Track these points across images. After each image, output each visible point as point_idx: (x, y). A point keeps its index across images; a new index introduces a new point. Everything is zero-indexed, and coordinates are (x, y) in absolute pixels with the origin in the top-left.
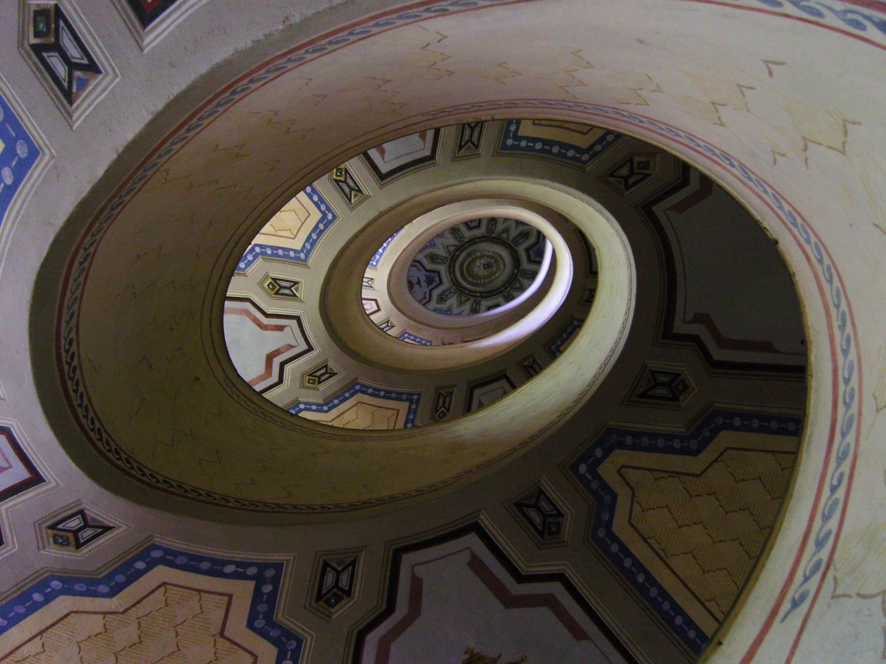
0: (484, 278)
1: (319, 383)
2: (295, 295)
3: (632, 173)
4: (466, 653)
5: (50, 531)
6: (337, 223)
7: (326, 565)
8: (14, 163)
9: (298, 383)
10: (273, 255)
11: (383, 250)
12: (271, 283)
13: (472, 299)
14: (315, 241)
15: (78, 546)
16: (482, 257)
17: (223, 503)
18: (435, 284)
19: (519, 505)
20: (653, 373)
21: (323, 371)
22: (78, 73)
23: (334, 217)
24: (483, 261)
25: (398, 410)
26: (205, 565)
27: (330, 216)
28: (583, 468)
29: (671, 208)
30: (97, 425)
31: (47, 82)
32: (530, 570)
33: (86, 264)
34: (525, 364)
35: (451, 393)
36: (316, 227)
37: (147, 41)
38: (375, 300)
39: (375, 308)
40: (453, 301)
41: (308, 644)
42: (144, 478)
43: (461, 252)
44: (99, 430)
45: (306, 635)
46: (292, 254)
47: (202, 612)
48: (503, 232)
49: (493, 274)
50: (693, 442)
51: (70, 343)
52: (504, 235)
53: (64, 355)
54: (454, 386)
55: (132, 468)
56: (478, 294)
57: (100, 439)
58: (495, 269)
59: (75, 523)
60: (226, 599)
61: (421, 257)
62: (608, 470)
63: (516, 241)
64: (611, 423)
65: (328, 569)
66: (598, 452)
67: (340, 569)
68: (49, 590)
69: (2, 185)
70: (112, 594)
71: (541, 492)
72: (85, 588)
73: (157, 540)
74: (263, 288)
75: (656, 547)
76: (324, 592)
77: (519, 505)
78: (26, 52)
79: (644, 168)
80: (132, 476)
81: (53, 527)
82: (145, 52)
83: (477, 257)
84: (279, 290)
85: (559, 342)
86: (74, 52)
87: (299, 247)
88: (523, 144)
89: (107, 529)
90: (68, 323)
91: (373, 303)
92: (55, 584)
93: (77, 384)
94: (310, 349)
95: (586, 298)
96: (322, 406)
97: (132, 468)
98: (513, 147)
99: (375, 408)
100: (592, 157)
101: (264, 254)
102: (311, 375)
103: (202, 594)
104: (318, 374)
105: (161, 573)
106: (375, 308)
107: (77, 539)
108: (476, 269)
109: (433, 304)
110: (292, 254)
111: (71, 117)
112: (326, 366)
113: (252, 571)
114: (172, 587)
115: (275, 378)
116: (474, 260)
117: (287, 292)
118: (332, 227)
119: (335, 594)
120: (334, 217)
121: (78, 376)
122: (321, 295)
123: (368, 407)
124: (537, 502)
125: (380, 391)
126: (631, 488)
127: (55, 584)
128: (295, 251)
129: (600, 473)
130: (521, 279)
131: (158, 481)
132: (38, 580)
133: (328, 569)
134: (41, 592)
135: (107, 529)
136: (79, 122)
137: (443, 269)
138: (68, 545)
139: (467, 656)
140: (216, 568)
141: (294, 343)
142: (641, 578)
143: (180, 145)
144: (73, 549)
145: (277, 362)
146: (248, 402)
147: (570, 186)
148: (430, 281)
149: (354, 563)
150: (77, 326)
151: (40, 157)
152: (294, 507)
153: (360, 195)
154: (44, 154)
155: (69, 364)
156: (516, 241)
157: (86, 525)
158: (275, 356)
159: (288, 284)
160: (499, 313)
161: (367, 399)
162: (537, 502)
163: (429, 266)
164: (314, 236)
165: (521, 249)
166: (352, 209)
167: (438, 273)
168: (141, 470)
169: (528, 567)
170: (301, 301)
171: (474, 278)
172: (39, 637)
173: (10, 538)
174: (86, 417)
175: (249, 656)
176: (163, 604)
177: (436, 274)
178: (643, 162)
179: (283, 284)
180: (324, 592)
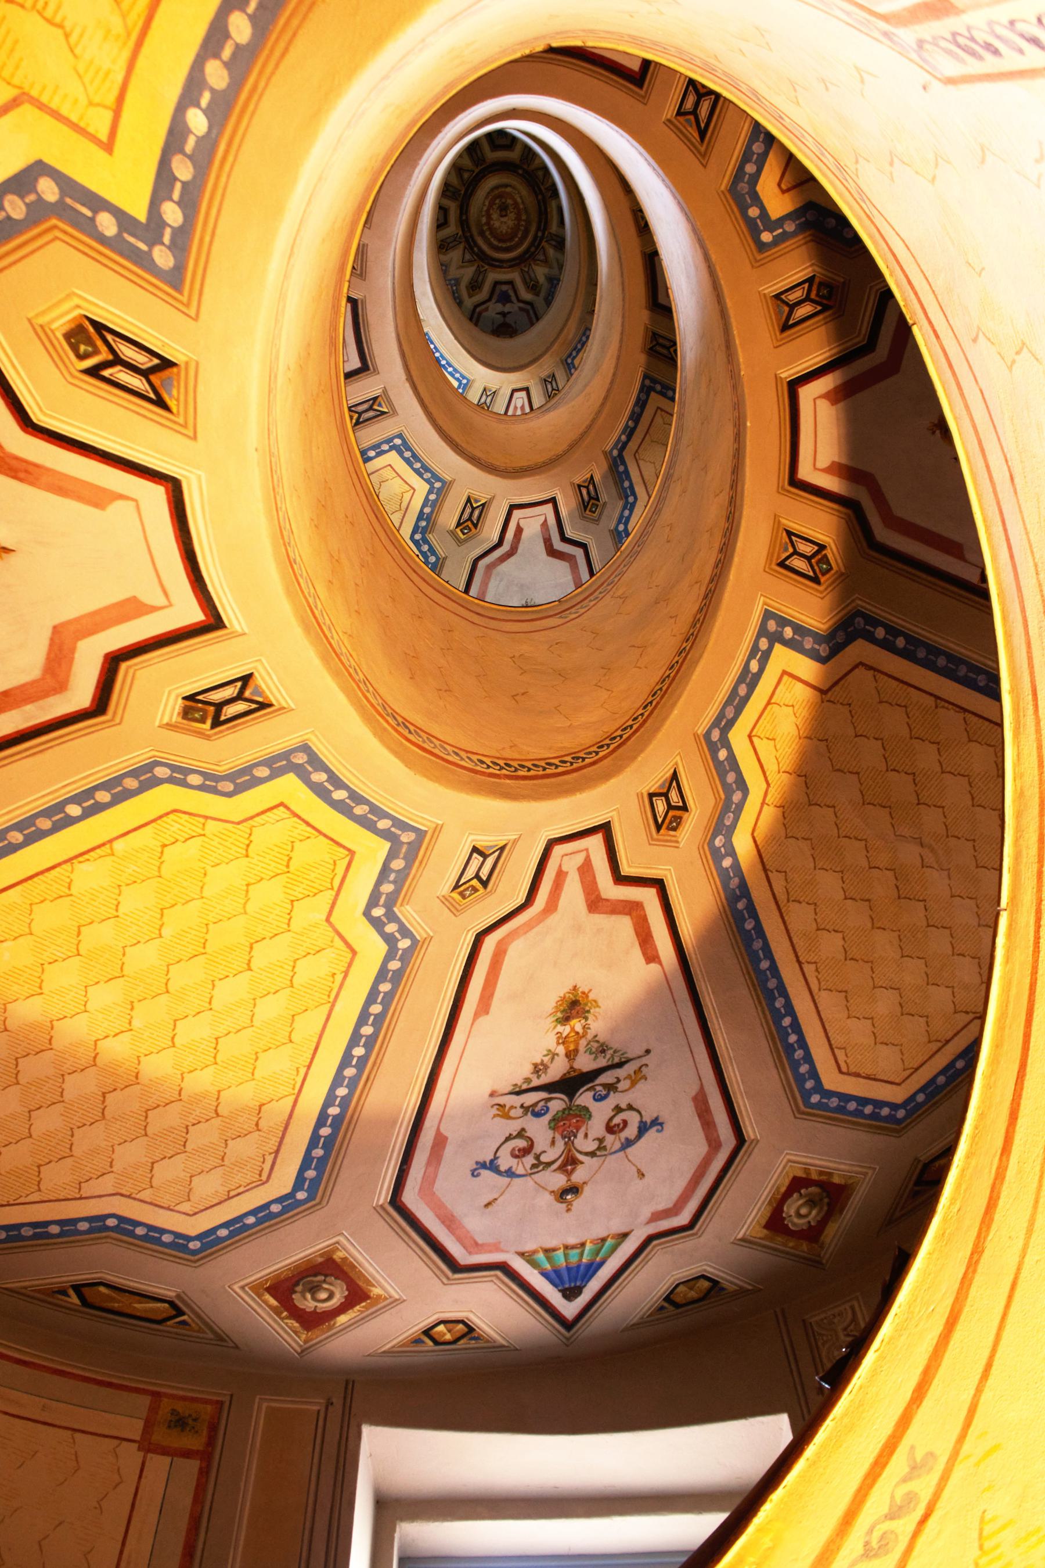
0: (518, 218)
1: (598, 499)
2: (483, 505)
4: (934, 433)
5: (662, 831)
6: (407, 435)
7: (782, 564)
8: (310, 769)
9: (592, 526)
11: (450, 366)
13: (544, 244)
15: (685, 808)
16: (489, 217)
17: (683, 655)
18: (511, 293)
19: (785, 327)
20: (680, 113)
22: (247, 694)
23: (400, 436)
24: (495, 216)
25: (658, 408)
26: (742, 690)
27: (398, 441)
28: (766, 237)
30: (569, 759)
31: (247, 721)
32: (863, 332)
33: (412, 728)
36: (407, 461)
37: (238, 628)
38: (514, 391)
39: (523, 394)
40: (540, 272)
41: (864, 604)
42: (635, 727)
43: (476, 244)
44: (573, 758)
45: (854, 605)
46: (432, 497)
47: (793, 706)
48: (461, 177)
49: (516, 203)
51: (482, 762)
52: (466, 175)
53: (491, 770)
55: (621, 736)
57: (584, 759)
58: (509, 201)
59: (661, 806)
60: (786, 678)
61: (469, 303)
64: (723, 188)
65: (787, 563)
66: (754, 212)
67: (791, 550)
68: (723, 850)
70: (745, 791)
71: (777, 297)
72: (731, 815)
73: (701, 730)
74: (465, 541)
76: (811, 574)
77: (785, 327)
78: (216, 734)
80: (629, 738)
81: (659, 827)
82: (246, 631)
83: (488, 223)
84: (472, 522)
86: (229, 692)
87: (427, 487)
89: (675, 776)
90: (462, 759)
91: (516, 395)
92: (719, 842)
93: (523, 766)
96: (627, 502)
97: (621, 736)
102: (585, 508)
103: (773, 701)
105: (737, 737)
106: (523, 394)
107: (678, 808)
108: (504, 229)
109: (539, 302)
110: (432, 497)
111: (284, 708)
112: (579, 486)
113: (764, 644)
114: (755, 730)
115: (578, 552)
116: (491, 229)
117: (477, 513)
118: (411, 441)
119: (818, 563)
120: (400, 436)
121: (515, 764)
122: (490, 473)
123: (642, 446)
124: (787, 304)
127: (719, 842)
128: (430, 492)
130: (532, 167)
131: (642, 715)
132: (709, 857)
133: (787, 563)
134: (723, 857)
135: (675, 776)
136: (290, 701)
137: (493, 276)
138: (681, 818)
139: (938, 432)
140: (749, 680)
141: (542, 518)
143: (326, 618)
144: (685, 815)
145: (558, 545)
146: (592, 598)
147: (428, 146)
148: (505, 298)
149: (790, 534)
150: (467, 752)
151: (310, 744)
152: (711, 581)
154: (858, 605)
155: (502, 768)
157: (666, 795)
158: (551, 545)
159: (468, 510)
160: (571, 221)
161: (632, 445)
162: (787, 304)
164: (418, 465)
166: (395, 412)
167: (496, 283)
168: (625, 729)
169: (859, 334)
171: (516, 236)
172: (769, 873)
173: (659, 872)
174: (557, 767)
175: (857, 670)
176: (772, 742)
179: (466, 516)
180: (811, 574)
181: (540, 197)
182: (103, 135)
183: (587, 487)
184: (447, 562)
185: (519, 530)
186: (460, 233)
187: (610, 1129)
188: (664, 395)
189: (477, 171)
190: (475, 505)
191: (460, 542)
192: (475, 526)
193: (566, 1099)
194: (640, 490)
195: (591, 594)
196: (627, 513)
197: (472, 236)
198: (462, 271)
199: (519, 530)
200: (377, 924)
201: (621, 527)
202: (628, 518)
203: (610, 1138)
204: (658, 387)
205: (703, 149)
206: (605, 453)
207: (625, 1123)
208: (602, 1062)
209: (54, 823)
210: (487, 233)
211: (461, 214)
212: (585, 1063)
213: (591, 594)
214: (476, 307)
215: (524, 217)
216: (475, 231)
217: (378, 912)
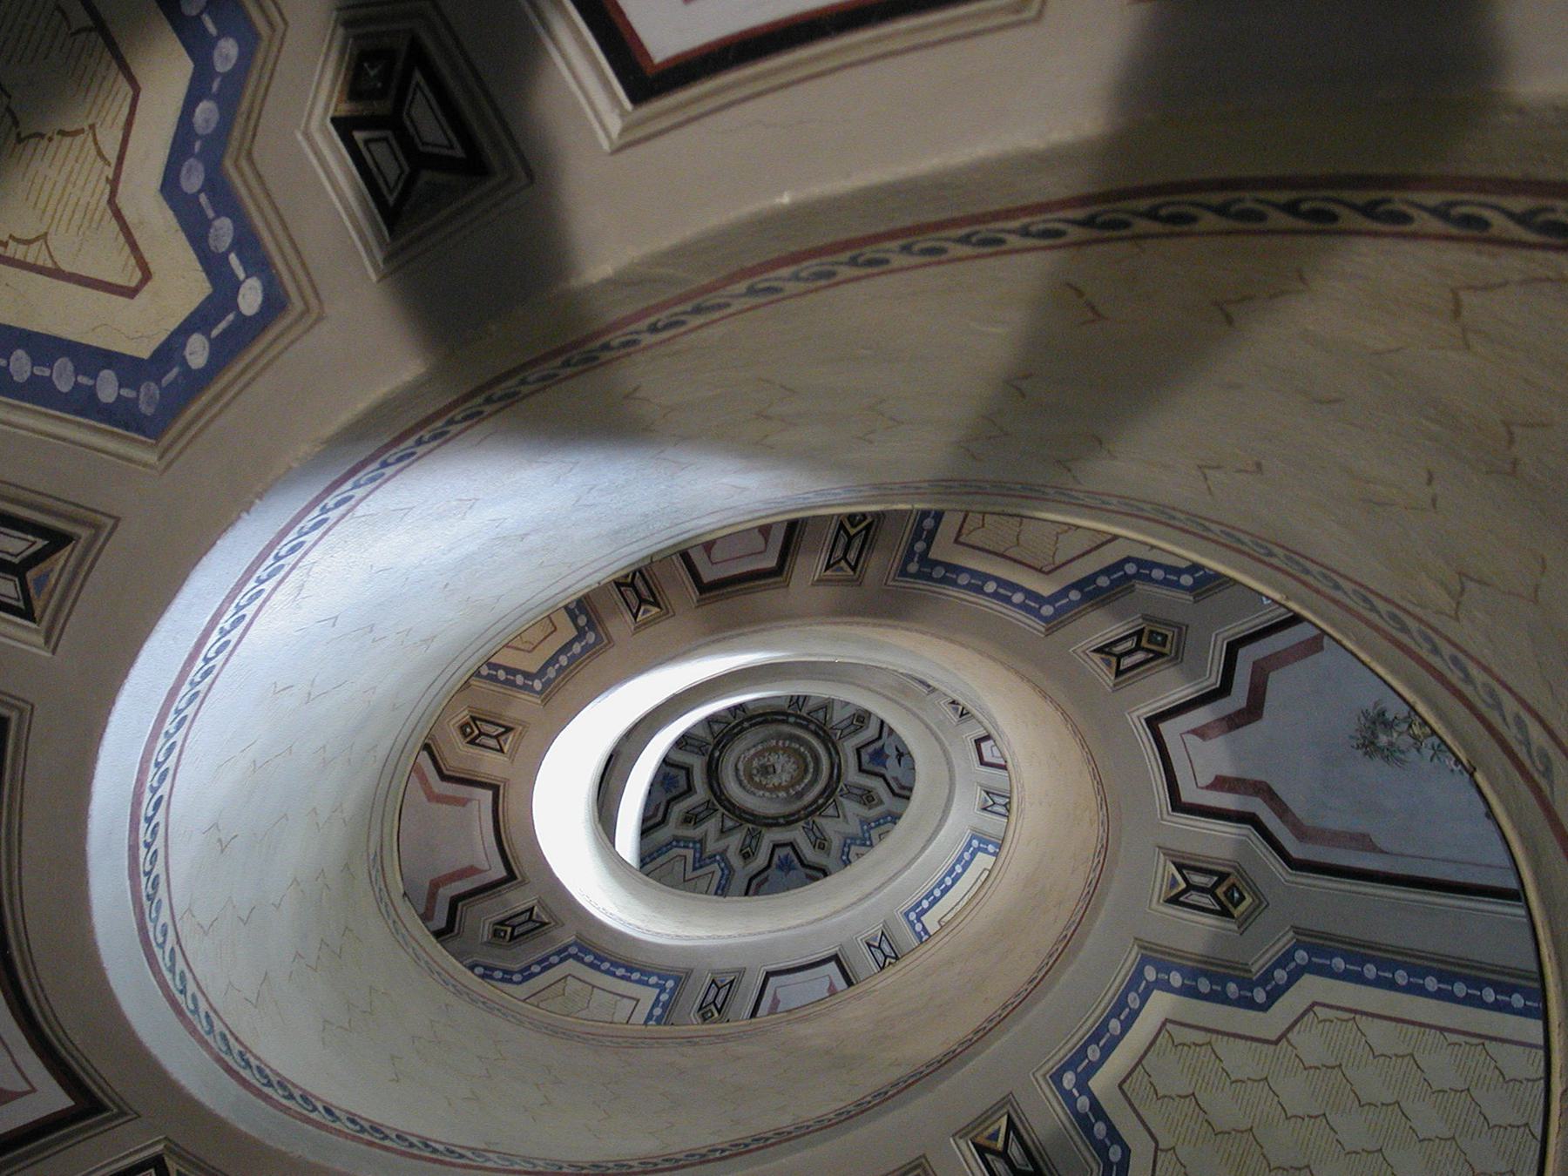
0: (774, 750)
2: (1180, 867)
6: (1052, 1064)
10: (1223, 980)
12: (1236, 906)
13: (804, 713)
14: (1115, 1013)
18: (871, 749)
21: (1127, 662)
24: (776, 781)
27: (1069, 1080)
28: (250, 298)
34: (655, 610)
40: (838, 716)
43: (815, 801)
48: (730, 829)
49: (758, 755)
52: (729, 824)
56: (792, 720)
62: (181, 285)
63: (709, 809)
64: (151, 457)
66: (197, 352)
70: (170, 186)
74: (1256, 894)
83: (786, 789)
88: (653, 980)
91: (987, 758)
94: (1153, 722)
95: (511, 736)
96: (1137, 576)
99: (1012, 553)
101: (1246, 984)
104: (1139, 656)
108: (791, 767)
112: (1119, 673)
115: (1247, 657)
117: (1197, 879)
118: (1063, 1052)
120: (1057, 1078)
125: (995, 595)
126: (118, 214)
129: (208, 285)
130: (709, 739)
137: (852, 775)
141: (1192, 740)
146: (1455, 677)
148: (879, 756)
153: (981, 1140)
156: (709, 809)
158: (1239, 713)
159: (1194, 898)
162: (411, 181)
163: (876, 785)
165: (701, 793)
166: (1008, 1100)
167: (861, 770)
170: (1168, 853)
171: (796, 751)
177: (865, 766)
181: (746, 725)
183: (1120, 657)
184: (1305, 924)
185: (1220, 783)
186: (802, 823)
188: (932, 535)
189: (722, 810)
190: (1183, 885)
191: (1260, 903)
192: (1223, 877)
194: (1109, 556)
195: (1440, 677)
196: (1158, 574)
197: (805, 808)
198: (849, 814)
199: (1220, 783)
200: (1274, 996)
201: (1186, 580)
202: (1168, 569)
204: (920, 546)
205: (84, 533)
206: (1049, 631)
210: (799, 788)
211: (777, 825)
213: (1440, 677)
214: (894, 794)
217: (1260, 996)
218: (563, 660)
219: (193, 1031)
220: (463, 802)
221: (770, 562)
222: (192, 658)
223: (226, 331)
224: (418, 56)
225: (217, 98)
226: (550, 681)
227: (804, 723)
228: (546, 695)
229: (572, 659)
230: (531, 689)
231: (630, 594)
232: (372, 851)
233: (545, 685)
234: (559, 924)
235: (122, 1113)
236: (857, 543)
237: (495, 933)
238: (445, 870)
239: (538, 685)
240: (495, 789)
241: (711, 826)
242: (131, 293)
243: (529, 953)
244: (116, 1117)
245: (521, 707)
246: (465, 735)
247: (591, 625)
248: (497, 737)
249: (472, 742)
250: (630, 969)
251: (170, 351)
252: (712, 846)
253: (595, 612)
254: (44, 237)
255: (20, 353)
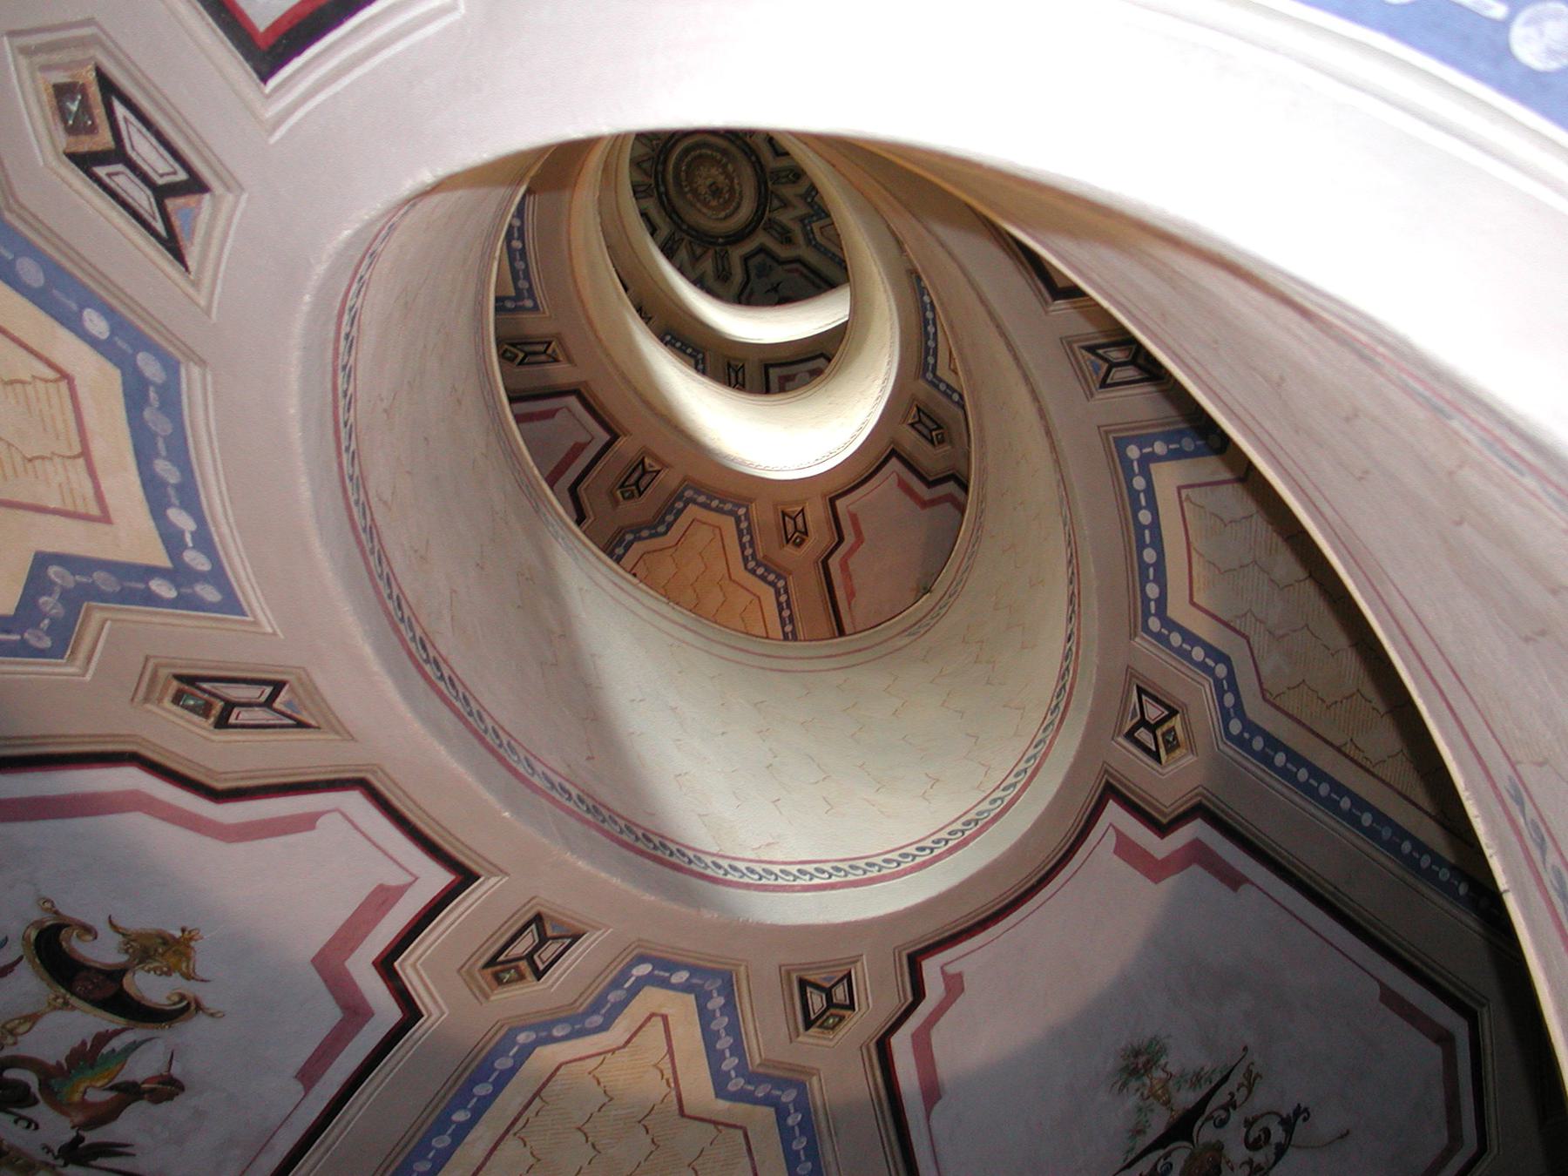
0: (695, 192)
3: (1152, 728)
4: (183, 930)
13: (652, 181)
16: (728, 176)
24: (722, 178)
28: (644, 969)
29: (1119, 834)
34: (647, 461)
35: (556, 360)
48: (781, 200)
49: (706, 204)
50: (742, 1081)
52: (776, 203)
54: (569, 360)
58: (714, 203)
62: (652, 998)
63: (771, 226)
66: (681, 977)
69: (1499, 11)
70: (603, 1028)
75: (530, 1112)
79: (1166, 742)
83: (724, 167)
85: (702, 499)
95: (789, 510)
98: (1126, 462)
100: (1158, 637)
108: (703, 171)
130: (711, 252)
137: (736, 254)
139: (178, 934)
142: (460, 1116)
156: (771, 226)
162: (555, 938)
165: (762, 238)
167: (746, 259)
178: (1175, 738)
182: (95, 511)
187: (1253, 1146)
189: (688, 238)
193: (1186, 1144)
203: (1259, 1157)
207: (1267, 1132)
208: (1206, 1089)
209: (494, 1084)
211: (758, 158)
212: (1186, 1098)
215: (689, 196)
216: (733, 149)
218: (715, 503)
219: (1046, 754)
220: (854, 519)
221: (573, 401)
222: (833, 887)
223: (663, 968)
224: (492, 962)
225: (550, 1031)
226: (735, 505)
227: (659, 176)
228: (745, 502)
229: (711, 498)
230: (747, 513)
231: (643, 483)
232: (906, 641)
233: (740, 506)
234: (914, 398)
235: (1106, 771)
236: (528, 348)
237: (941, 442)
238: (910, 504)
239: (742, 511)
240: (832, 501)
241: (785, 217)
242: (665, 1018)
243: (945, 409)
244: (1111, 775)
245: (763, 515)
246: (803, 541)
247: (680, 497)
248: (794, 519)
249: (806, 533)
250: (926, 322)
251: (686, 988)
252: (802, 210)
253: (671, 495)
254: (655, 1066)
255: (718, 1046)
